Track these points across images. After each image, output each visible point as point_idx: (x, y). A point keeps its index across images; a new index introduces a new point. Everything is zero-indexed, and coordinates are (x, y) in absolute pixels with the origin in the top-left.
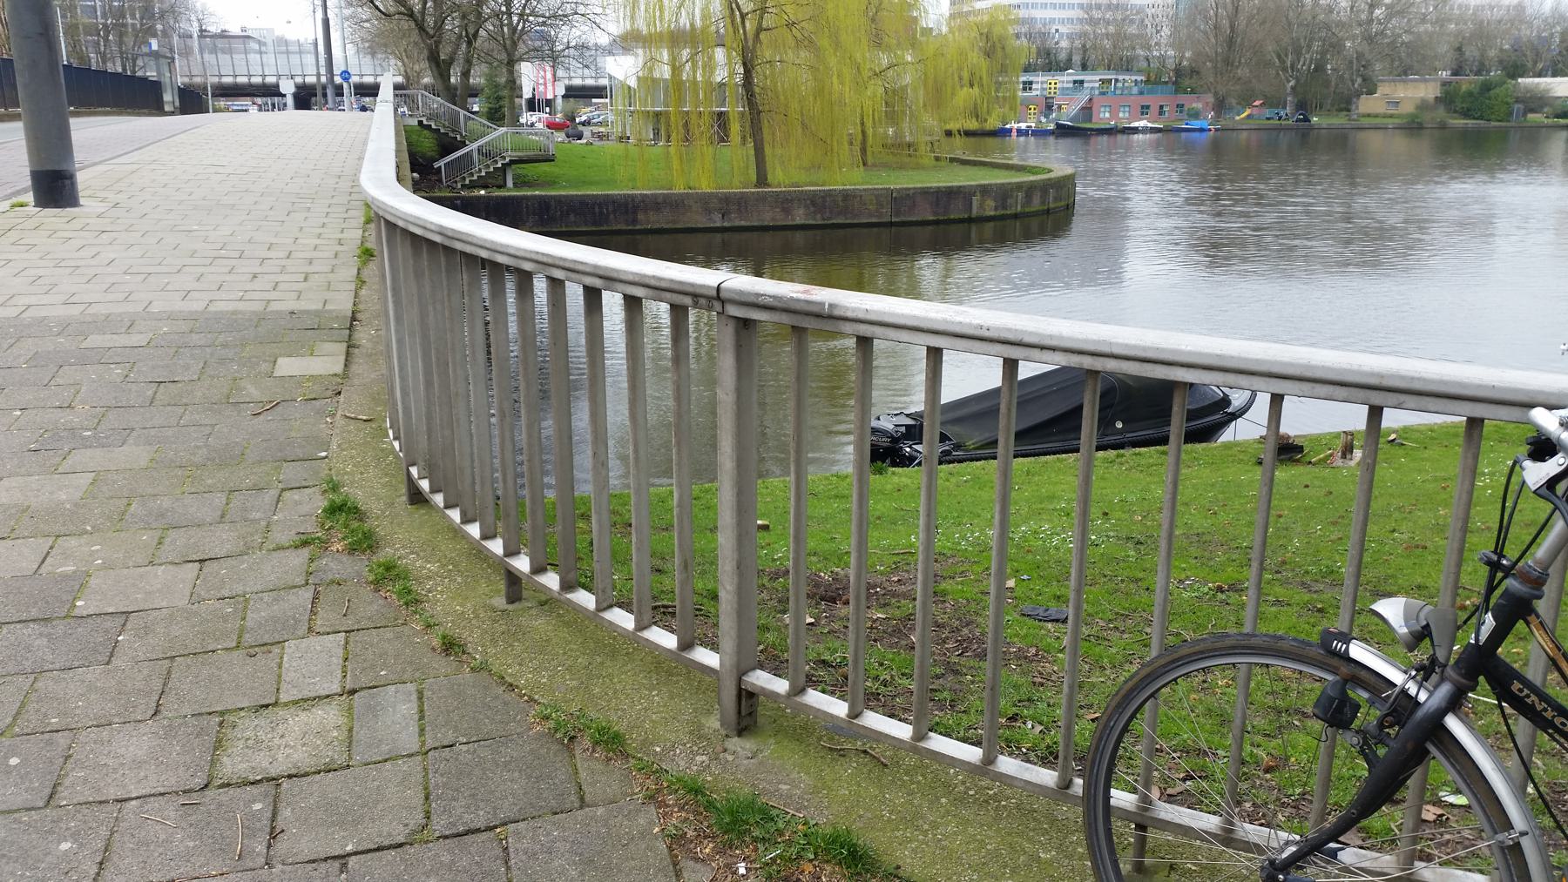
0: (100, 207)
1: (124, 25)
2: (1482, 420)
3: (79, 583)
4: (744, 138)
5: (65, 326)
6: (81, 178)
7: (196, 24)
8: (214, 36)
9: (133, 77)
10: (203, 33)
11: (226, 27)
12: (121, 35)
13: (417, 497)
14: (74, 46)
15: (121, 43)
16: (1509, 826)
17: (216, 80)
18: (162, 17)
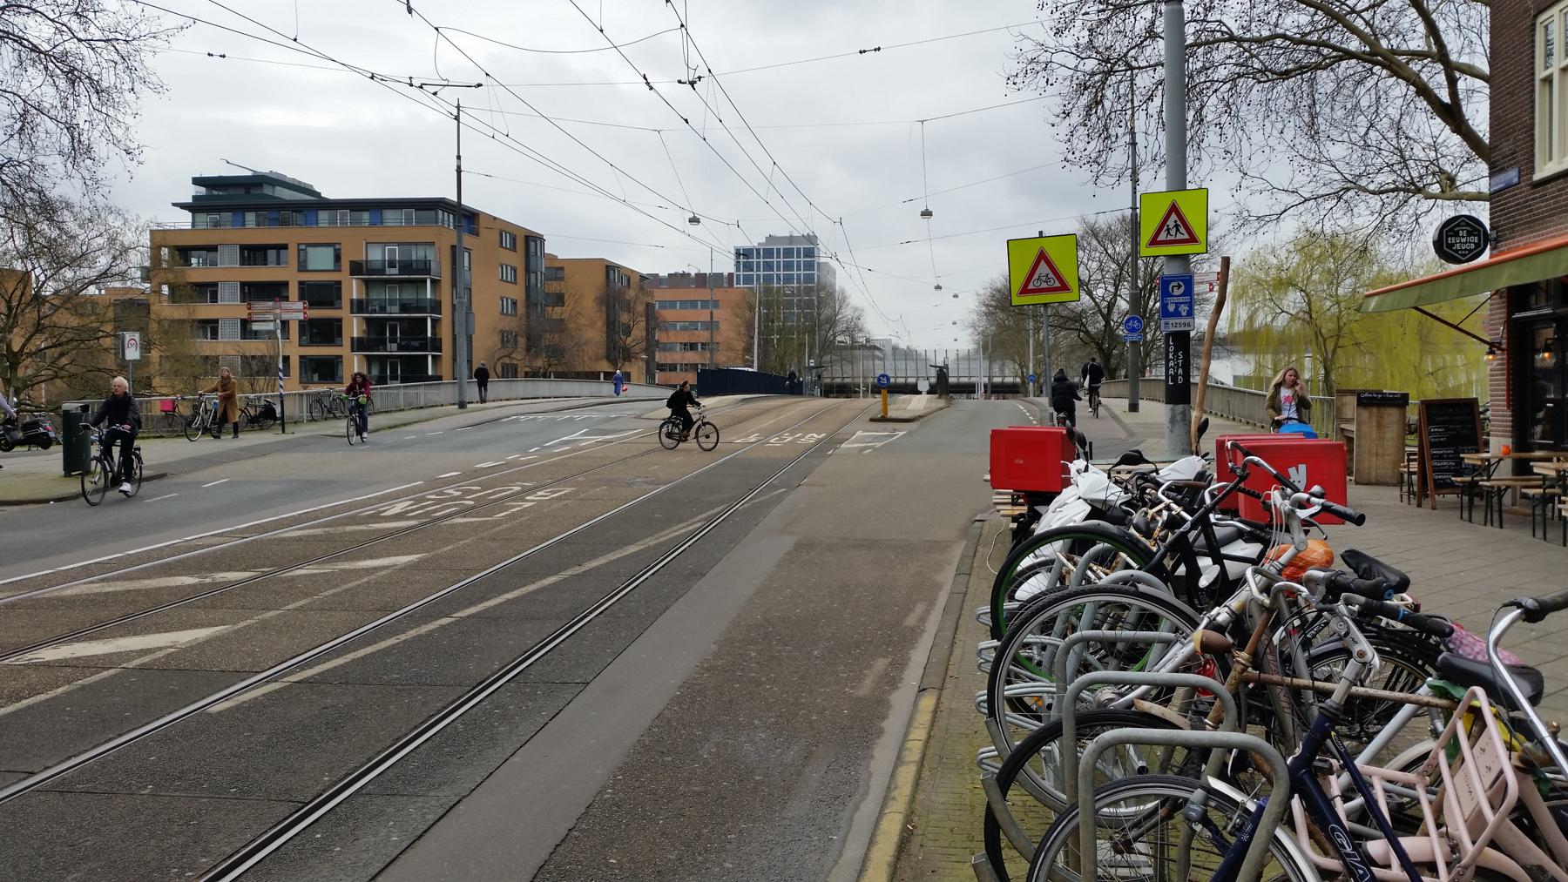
18: (116, 336)
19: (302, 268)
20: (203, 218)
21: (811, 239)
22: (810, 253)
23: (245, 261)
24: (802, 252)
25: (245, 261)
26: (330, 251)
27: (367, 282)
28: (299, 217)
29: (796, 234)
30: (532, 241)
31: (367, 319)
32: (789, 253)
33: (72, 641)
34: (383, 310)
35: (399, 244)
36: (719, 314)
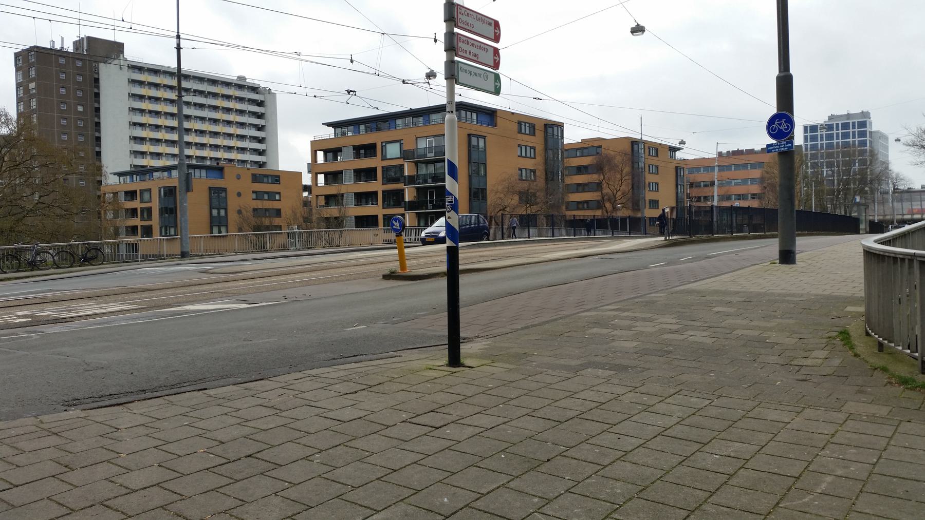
0: (803, 264)
1: (849, 189)
2: (341, 172)
3: (768, 338)
4: (135, 166)
5: (779, 295)
6: (798, 256)
7: (891, 186)
8: (903, 192)
9: (850, 217)
10: (896, 190)
11: (911, 186)
12: (846, 194)
13: (868, 334)
14: (819, 199)
15: (845, 199)
16: (374, 170)
17: (900, 217)
18: (871, 183)
19: (384, 158)
20: (339, 130)
21: (866, 114)
22: (863, 124)
23: (357, 155)
24: (862, 122)
25: (357, 155)
26: (398, 145)
27: (417, 163)
28: (386, 125)
29: (852, 112)
30: (552, 129)
31: (417, 189)
32: (846, 126)
33: (847, 298)
34: (426, 182)
35: (434, 136)
36: (228, 182)
